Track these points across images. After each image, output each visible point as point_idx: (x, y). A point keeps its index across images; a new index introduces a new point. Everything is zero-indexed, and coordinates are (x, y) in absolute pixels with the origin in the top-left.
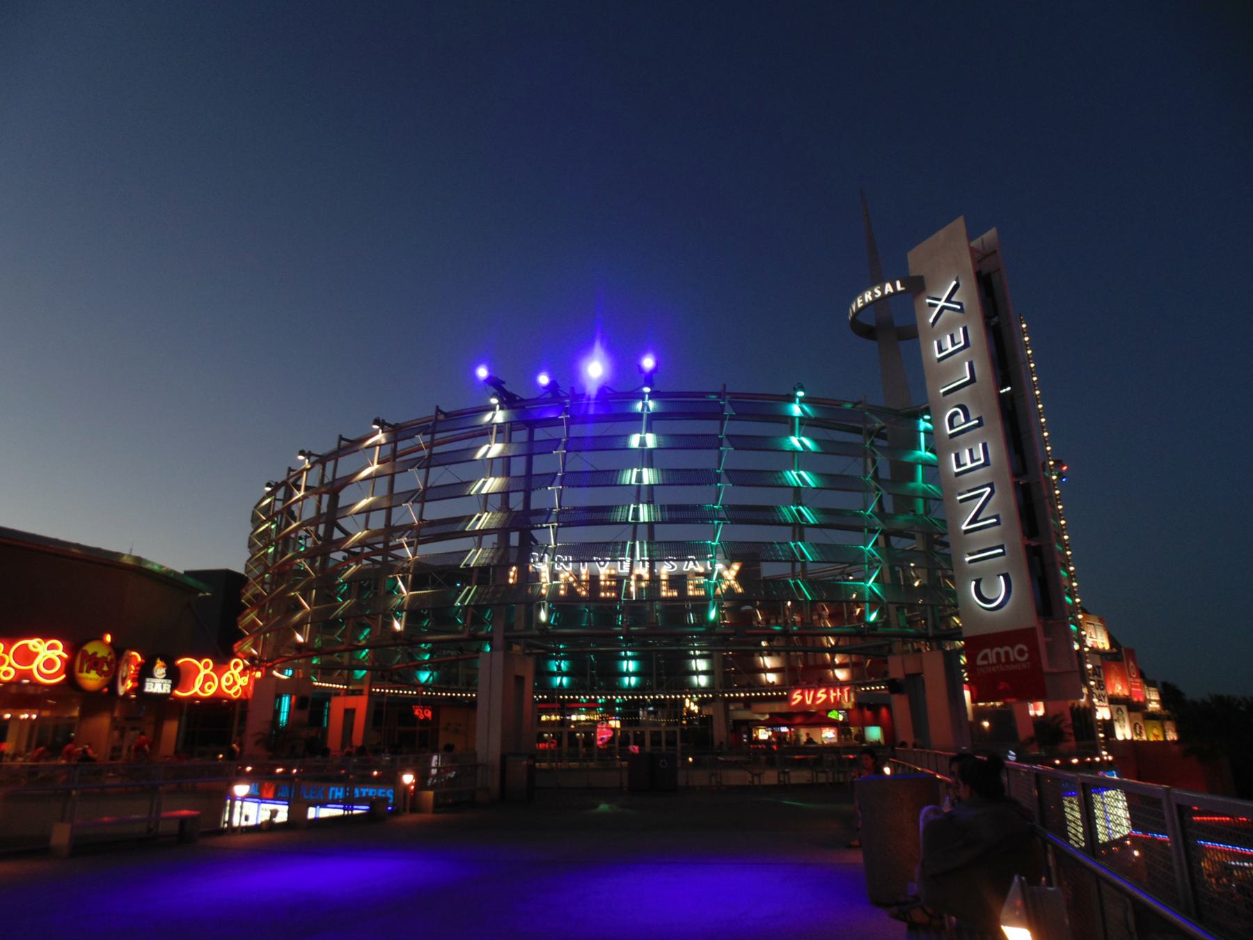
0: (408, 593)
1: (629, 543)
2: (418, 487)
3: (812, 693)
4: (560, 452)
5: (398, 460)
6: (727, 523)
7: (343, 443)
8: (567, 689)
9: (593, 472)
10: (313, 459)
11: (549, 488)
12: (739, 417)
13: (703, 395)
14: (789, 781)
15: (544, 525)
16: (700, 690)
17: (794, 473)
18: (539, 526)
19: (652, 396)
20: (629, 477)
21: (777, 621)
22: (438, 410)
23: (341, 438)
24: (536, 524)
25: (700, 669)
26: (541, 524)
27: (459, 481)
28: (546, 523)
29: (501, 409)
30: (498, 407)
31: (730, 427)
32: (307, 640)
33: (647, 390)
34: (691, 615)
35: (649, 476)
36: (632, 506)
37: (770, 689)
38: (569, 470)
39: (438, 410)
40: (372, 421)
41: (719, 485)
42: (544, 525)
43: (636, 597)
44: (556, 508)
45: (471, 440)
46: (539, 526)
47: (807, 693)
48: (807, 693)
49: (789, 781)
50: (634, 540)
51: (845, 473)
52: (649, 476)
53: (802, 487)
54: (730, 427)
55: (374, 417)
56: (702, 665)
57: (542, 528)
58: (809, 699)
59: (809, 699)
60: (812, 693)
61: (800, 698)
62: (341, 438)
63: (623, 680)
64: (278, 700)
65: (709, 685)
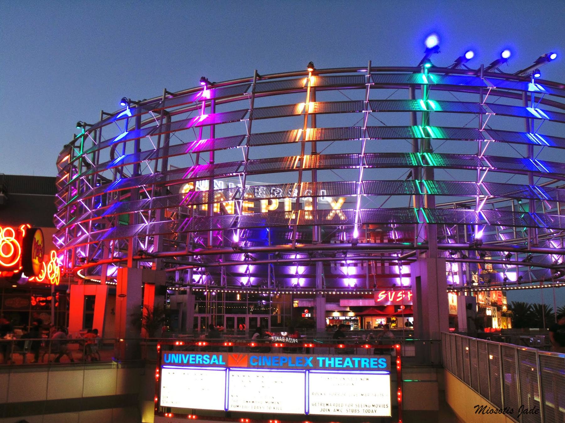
0: (149, 223)
1: (296, 184)
2: (152, 149)
3: (394, 293)
4: (246, 120)
5: (142, 128)
6: (365, 168)
7: (105, 116)
8: (302, 287)
9: (182, 145)
10: (87, 128)
11: (238, 147)
12: (377, 86)
13: (355, 70)
14: (405, 355)
15: (234, 174)
16: (350, 289)
17: (420, 128)
18: (231, 174)
19: (314, 73)
20: (297, 134)
21: (375, 241)
22: (166, 92)
23: (103, 113)
24: (229, 173)
25: (350, 274)
26: (232, 173)
27: (182, 143)
28: (235, 172)
29: (207, 89)
30: (205, 87)
31: (369, 94)
32: (87, 255)
33: (310, 70)
34: (345, 233)
35: (310, 133)
36: (298, 157)
37: (452, 288)
38: (219, 137)
39: (166, 92)
40: (120, 101)
41: (361, 139)
42: (234, 174)
43: (299, 224)
44: (244, 161)
45: (189, 113)
46: (231, 174)
47: (389, 293)
48: (389, 293)
49: (405, 355)
50: (300, 182)
51: (467, 127)
52: (310, 133)
53: (424, 138)
54: (369, 94)
55: (122, 98)
56: (352, 270)
57: (233, 176)
58: (391, 298)
59: (391, 298)
60: (394, 293)
61: (384, 296)
62: (103, 113)
63: (290, 281)
64: (42, 296)
65: (411, 282)
